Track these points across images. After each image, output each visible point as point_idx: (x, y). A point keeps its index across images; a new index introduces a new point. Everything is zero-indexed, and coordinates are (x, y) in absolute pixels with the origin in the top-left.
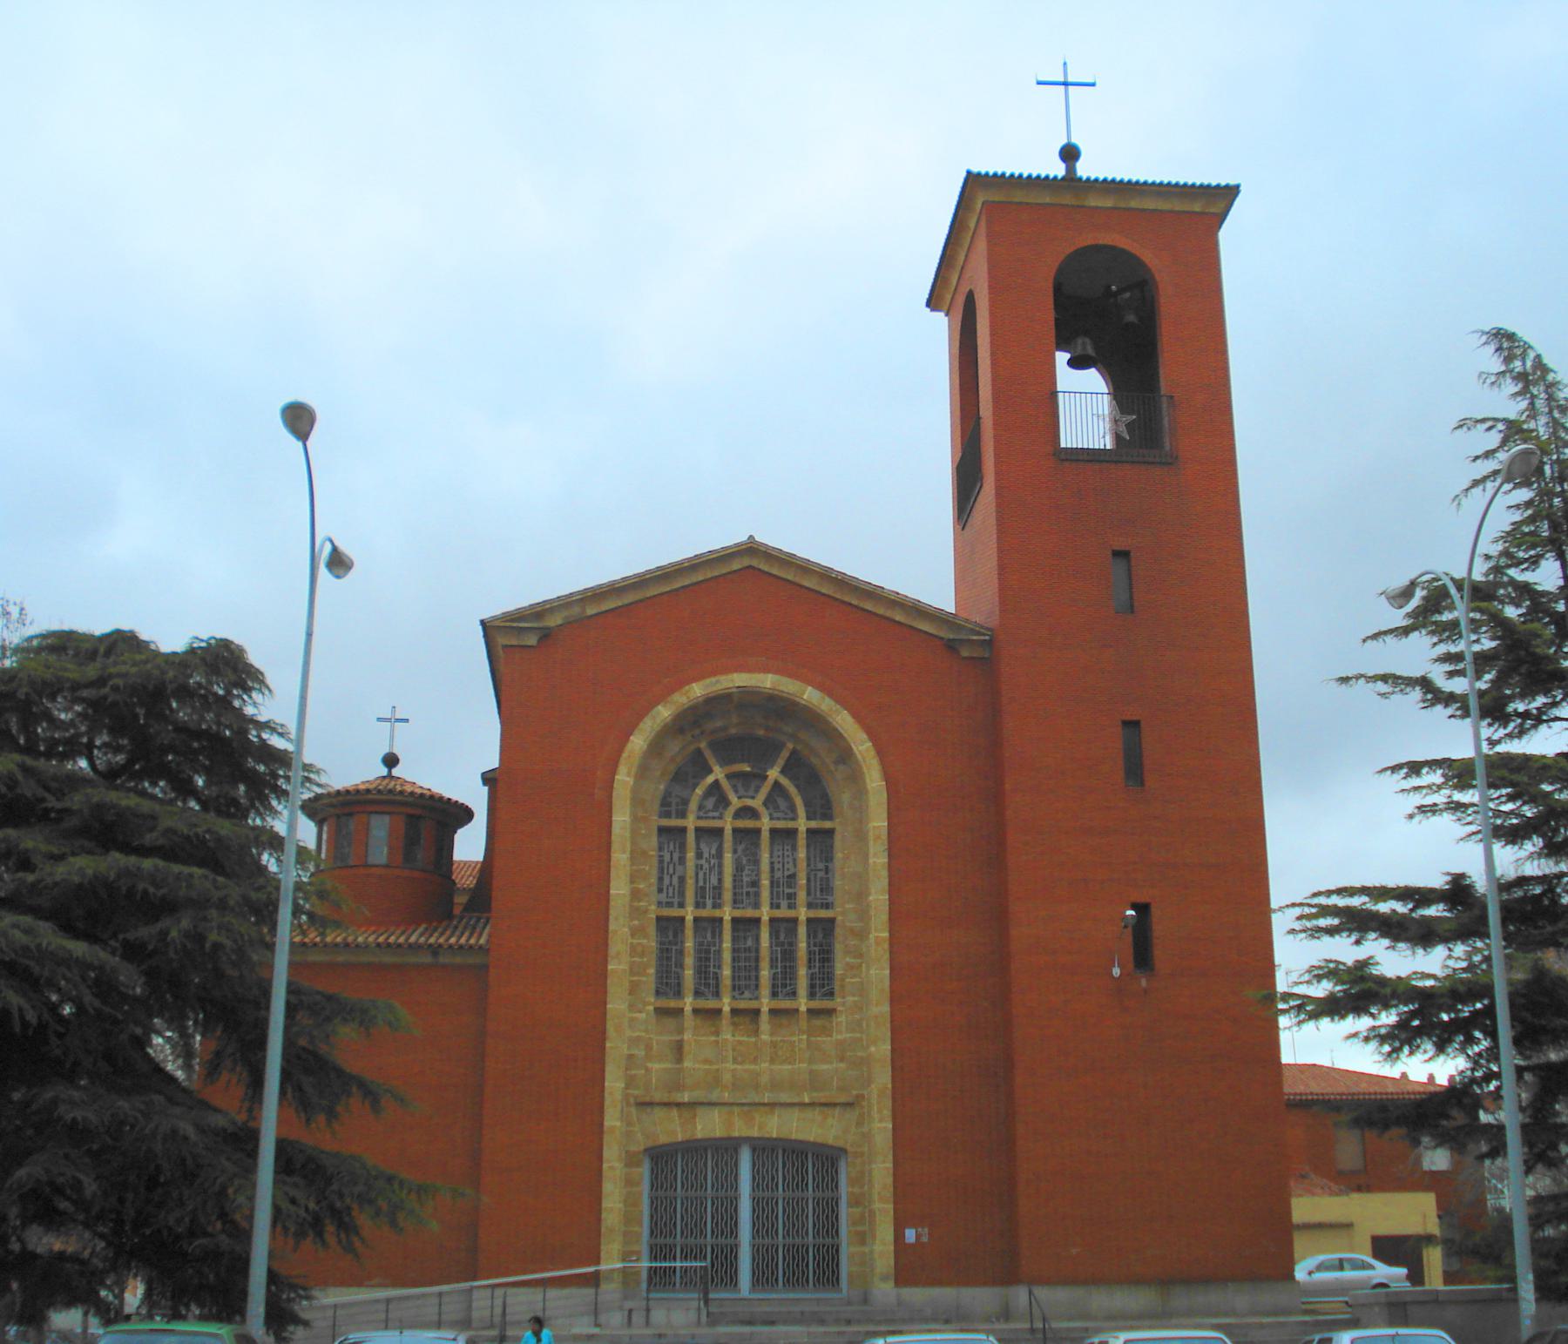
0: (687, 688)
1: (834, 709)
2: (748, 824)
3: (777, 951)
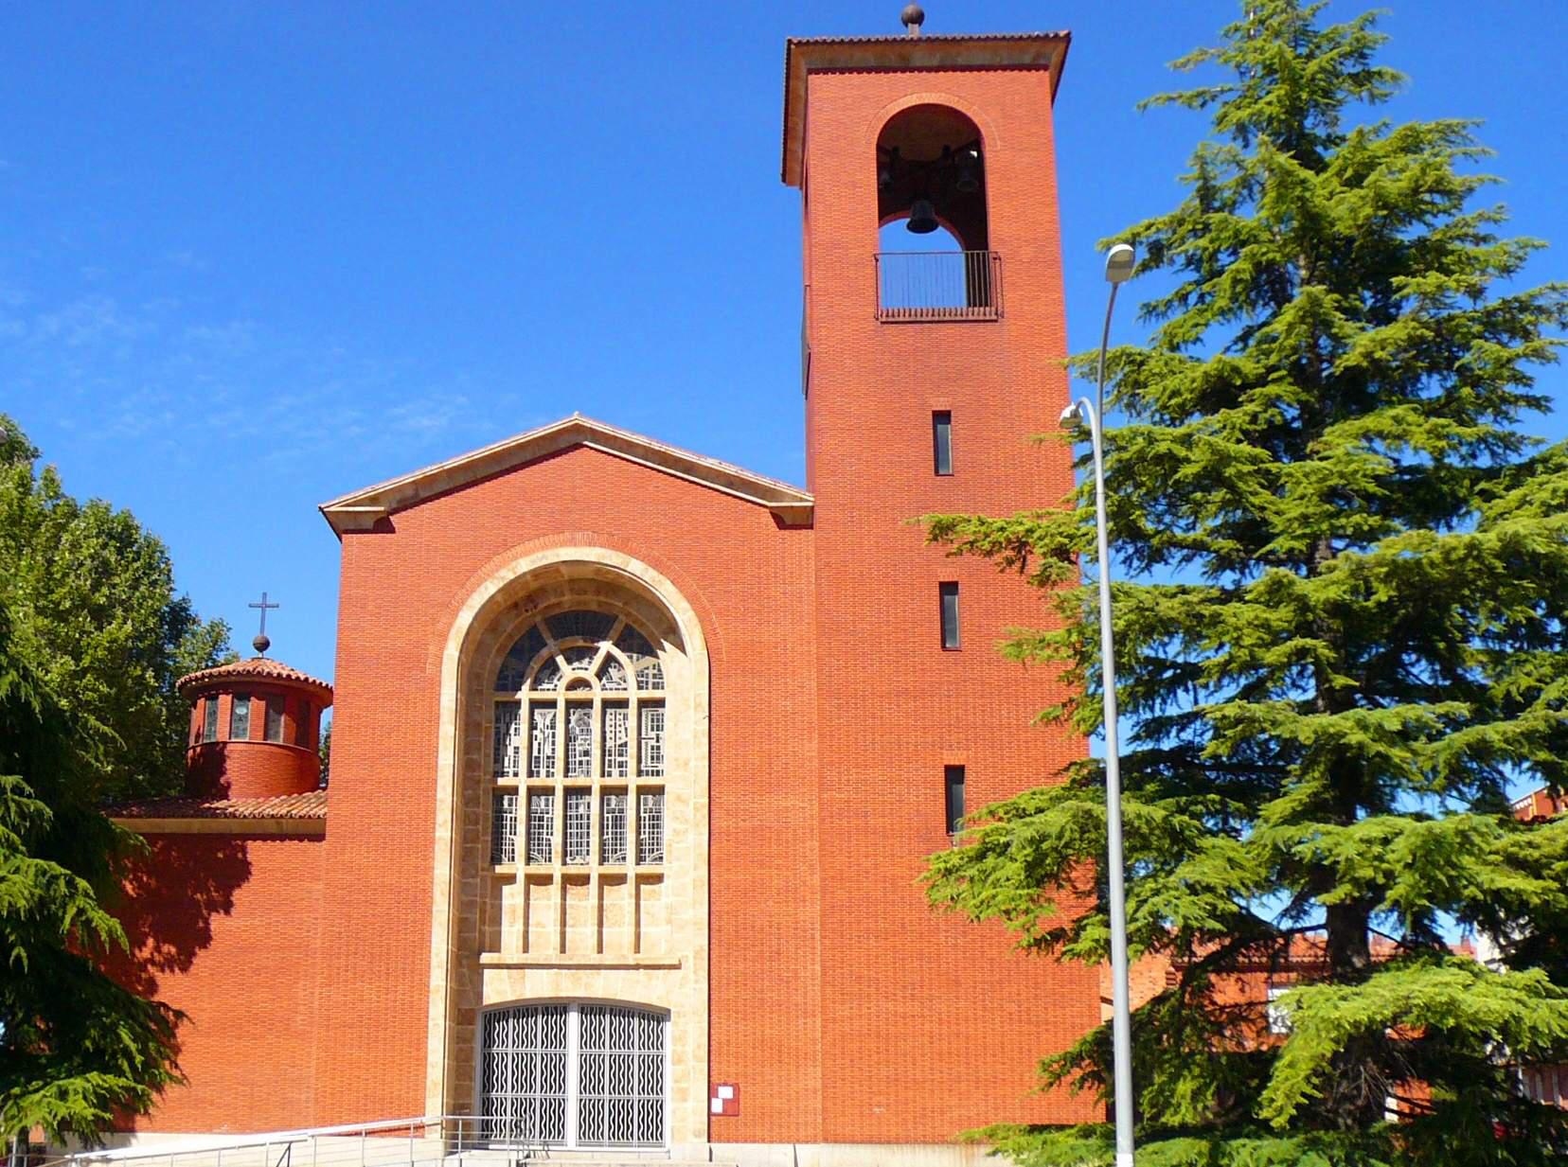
2: (580, 694)
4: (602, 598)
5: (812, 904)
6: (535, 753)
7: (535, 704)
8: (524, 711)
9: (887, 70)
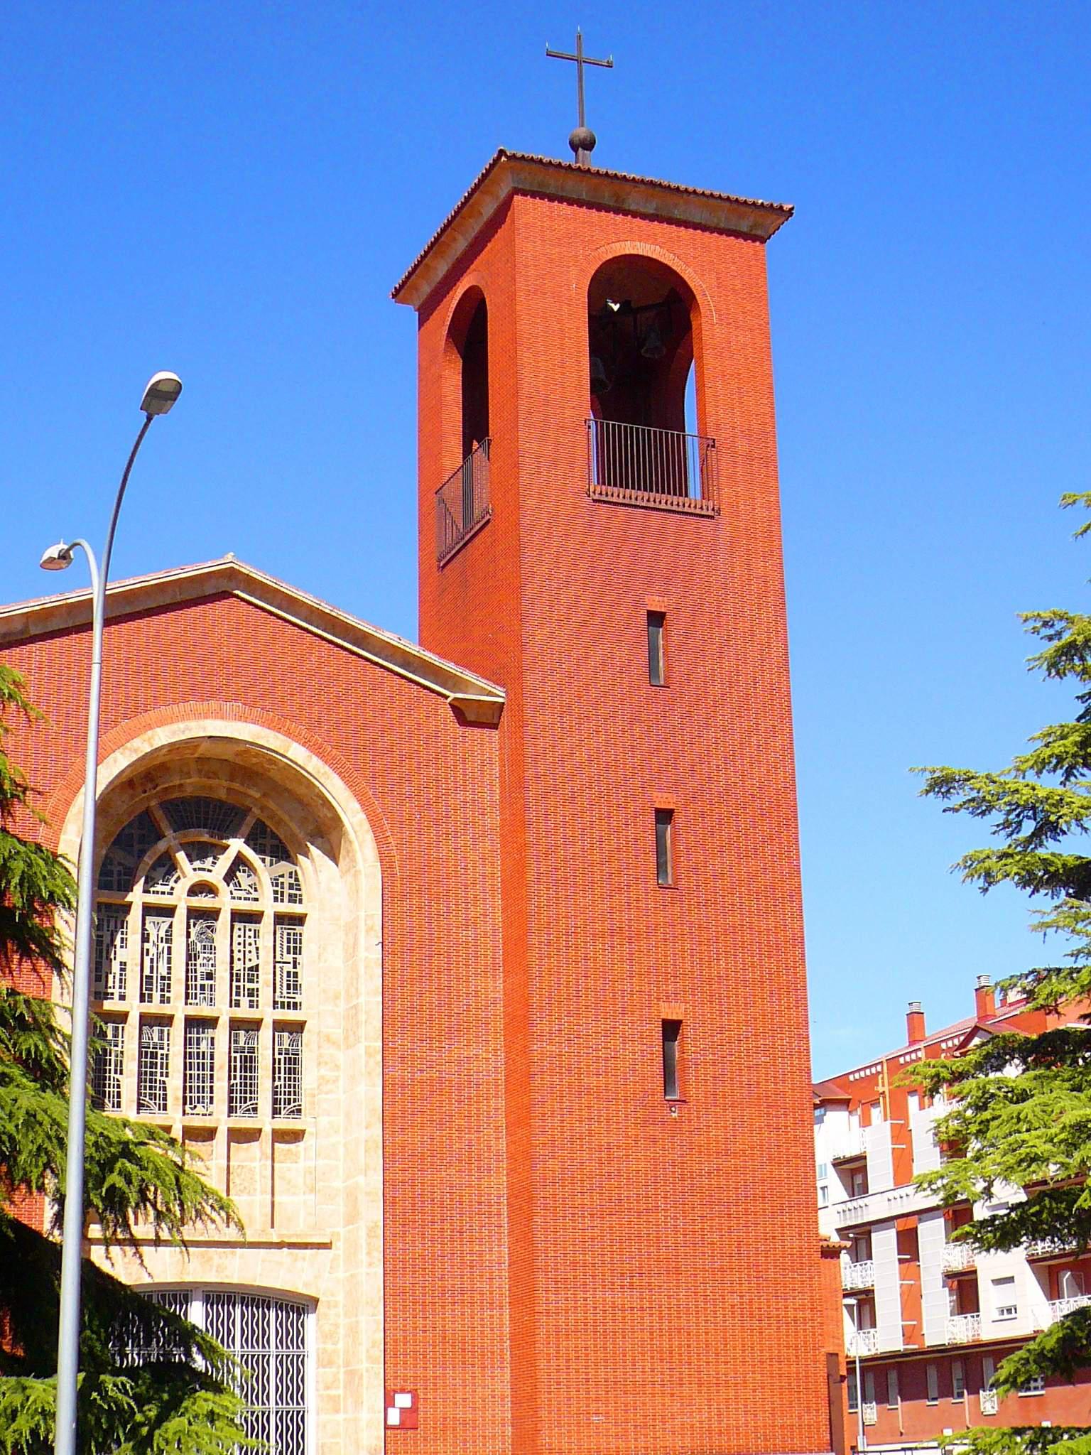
2: (203, 901)
4: (236, 786)
5: (498, 1173)
6: (147, 972)
7: (148, 910)
8: (135, 917)
9: (600, 207)
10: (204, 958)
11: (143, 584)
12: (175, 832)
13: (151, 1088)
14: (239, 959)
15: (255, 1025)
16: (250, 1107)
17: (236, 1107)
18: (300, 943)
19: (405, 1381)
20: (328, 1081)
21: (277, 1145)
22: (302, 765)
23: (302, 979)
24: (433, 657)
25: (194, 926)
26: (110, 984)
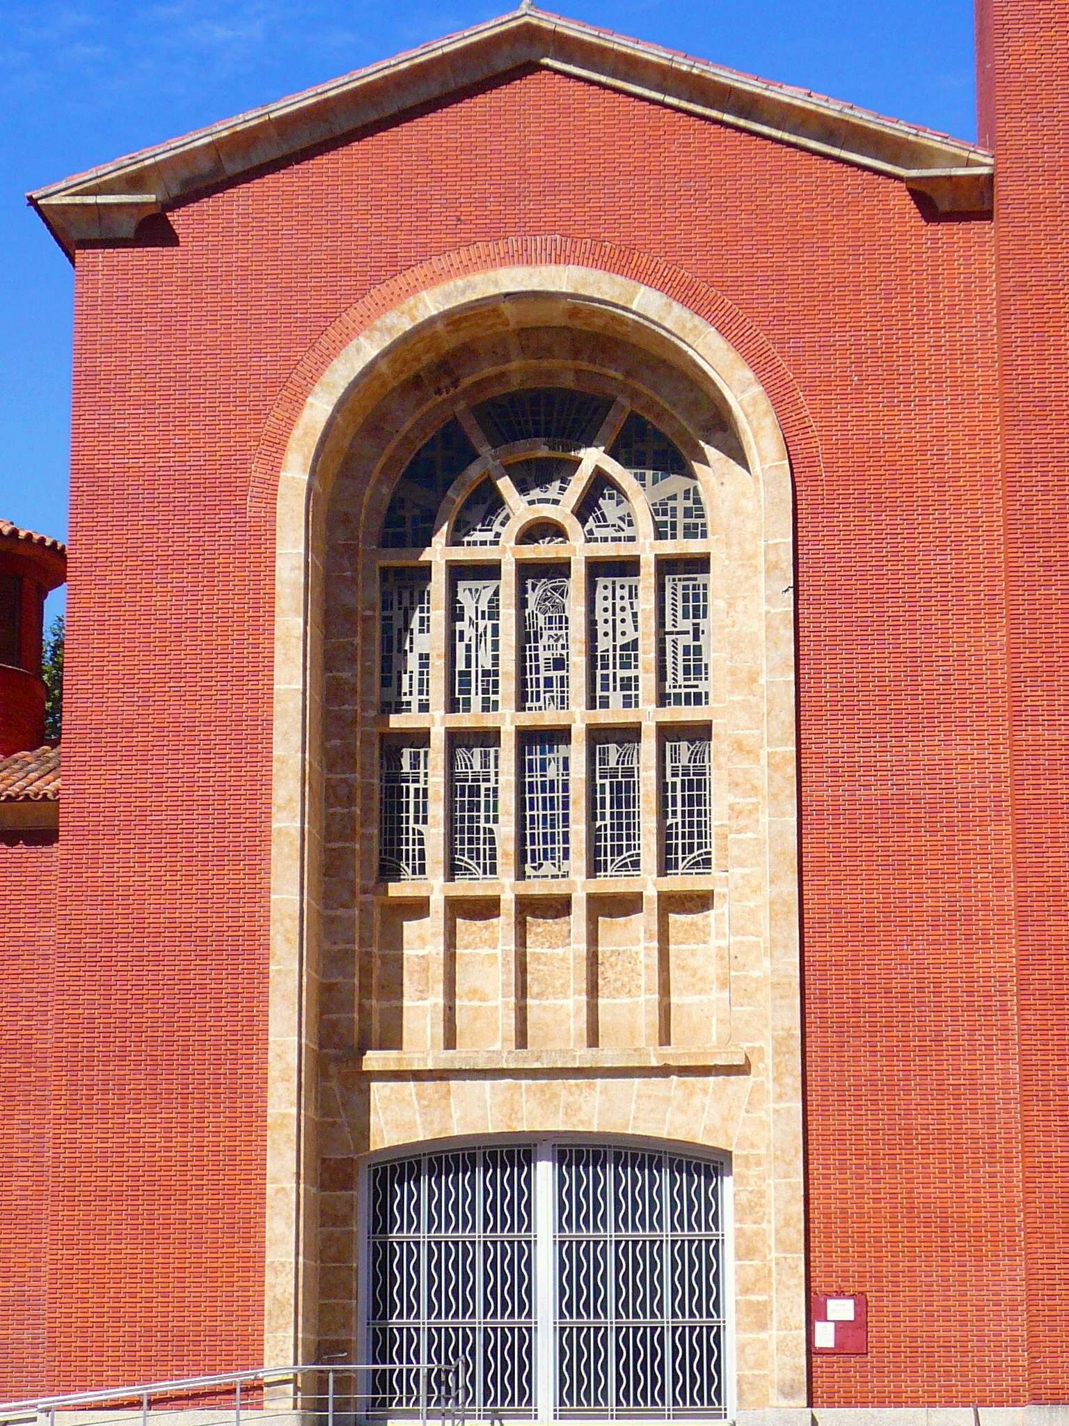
0: (411, 301)
1: (689, 325)
2: (544, 550)
3: (603, 786)
4: (585, 365)
6: (460, 666)
7: (457, 572)
8: (438, 585)
10: (550, 636)
11: (387, 72)
12: (494, 447)
13: (471, 841)
14: (606, 634)
15: (631, 734)
16: (628, 860)
17: (606, 861)
18: (705, 600)
19: (845, 1279)
20: (740, 812)
21: (673, 917)
22: (656, 319)
23: (709, 657)
24: (865, 117)
25: (533, 590)
26: (405, 689)
